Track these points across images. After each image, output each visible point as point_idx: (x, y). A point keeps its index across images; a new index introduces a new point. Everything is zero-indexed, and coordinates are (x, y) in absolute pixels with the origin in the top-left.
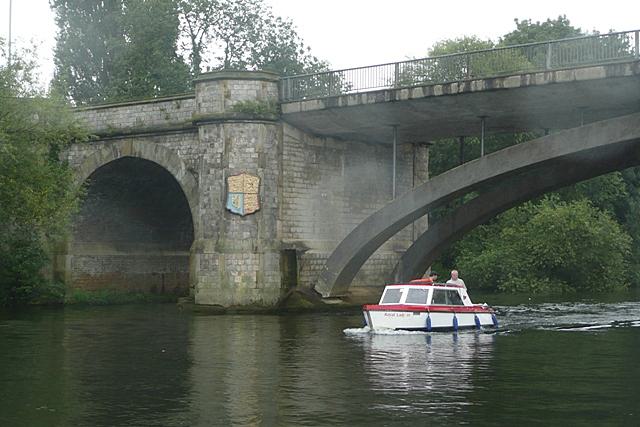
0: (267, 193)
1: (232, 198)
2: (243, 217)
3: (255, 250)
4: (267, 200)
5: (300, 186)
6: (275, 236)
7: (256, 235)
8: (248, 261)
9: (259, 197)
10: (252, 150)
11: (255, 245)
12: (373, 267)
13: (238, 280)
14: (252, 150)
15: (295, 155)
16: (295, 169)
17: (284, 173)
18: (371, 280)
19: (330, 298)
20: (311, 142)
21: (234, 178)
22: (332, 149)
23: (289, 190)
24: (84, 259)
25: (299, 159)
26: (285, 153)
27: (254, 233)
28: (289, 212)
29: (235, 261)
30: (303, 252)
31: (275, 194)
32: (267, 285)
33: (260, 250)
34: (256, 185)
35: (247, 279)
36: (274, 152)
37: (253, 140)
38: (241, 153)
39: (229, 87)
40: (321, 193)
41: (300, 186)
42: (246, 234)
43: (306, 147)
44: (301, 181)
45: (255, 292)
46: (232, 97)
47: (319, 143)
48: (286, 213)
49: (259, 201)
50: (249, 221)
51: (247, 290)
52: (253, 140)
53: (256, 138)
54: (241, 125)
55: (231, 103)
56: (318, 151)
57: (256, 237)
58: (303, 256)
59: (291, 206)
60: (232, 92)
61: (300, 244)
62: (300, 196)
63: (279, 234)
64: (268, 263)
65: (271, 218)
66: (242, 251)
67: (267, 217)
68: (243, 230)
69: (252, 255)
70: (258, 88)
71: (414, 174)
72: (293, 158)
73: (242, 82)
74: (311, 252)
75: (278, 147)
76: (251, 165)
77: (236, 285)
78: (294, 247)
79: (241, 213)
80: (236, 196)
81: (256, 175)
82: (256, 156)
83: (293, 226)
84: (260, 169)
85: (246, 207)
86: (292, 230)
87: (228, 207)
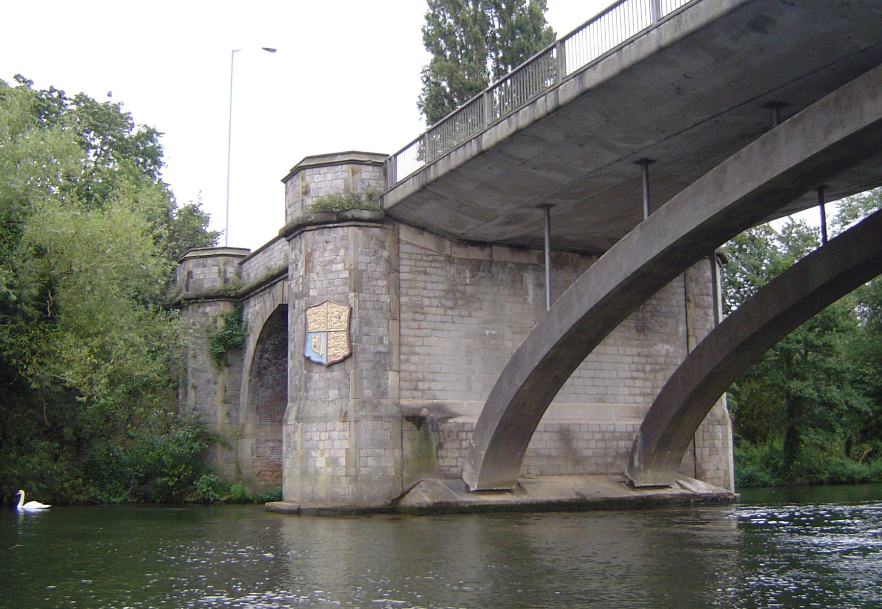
0: (365, 329)
1: (313, 340)
2: (330, 366)
3: (344, 417)
4: (365, 339)
5: (438, 318)
6: (384, 394)
7: (347, 394)
8: (335, 435)
9: (349, 335)
10: (340, 266)
11: (344, 410)
12: (600, 445)
13: (321, 463)
14: (340, 266)
15: (425, 273)
16: (425, 293)
17: (403, 299)
18: (597, 464)
19: (479, 492)
20: (461, 253)
21: (316, 310)
22: (505, 263)
23: (415, 325)
24: (271, 444)
25: (435, 278)
26: (402, 269)
27: (344, 392)
28: (414, 359)
29: (316, 433)
30: (444, 420)
31: (382, 331)
32: (363, 471)
33: (351, 415)
34: (345, 317)
35: (333, 462)
36: (381, 268)
37: (342, 252)
38: (326, 272)
39: (308, 179)
40: (485, 329)
41: (438, 318)
42: (333, 393)
43: (450, 260)
44: (441, 311)
45: (344, 482)
46: (312, 194)
47: (476, 253)
48: (408, 361)
49: (350, 341)
50: (337, 373)
51: (335, 479)
52: (342, 252)
53: (347, 249)
54: (326, 231)
55: (310, 201)
56: (476, 266)
57: (347, 397)
58: (443, 427)
59: (418, 350)
60: (312, 186)
61: (439, 408)
62: (439, 334)
63: (392, 393)
64: (365, 436)
65: (374, 368)
66: (326, 419)
67: (365, 366)
68: (329, 387)
69: (339, 425)
70: (346, 175)
71: (687, 300)
72: (421, 277)
73: (325, 170)
74: (460, 420)
75: (388, 261)
76: (340, 289)
77: (317, 471)
78: (424, 412)
79: (324, 361)
80: (318, 336)
81: (346, 302)
82: (346, 274)
83: (419, 380)
84: (352, 294)
85: (332, 351)
86: (421, 385)
87: (307, 355)
